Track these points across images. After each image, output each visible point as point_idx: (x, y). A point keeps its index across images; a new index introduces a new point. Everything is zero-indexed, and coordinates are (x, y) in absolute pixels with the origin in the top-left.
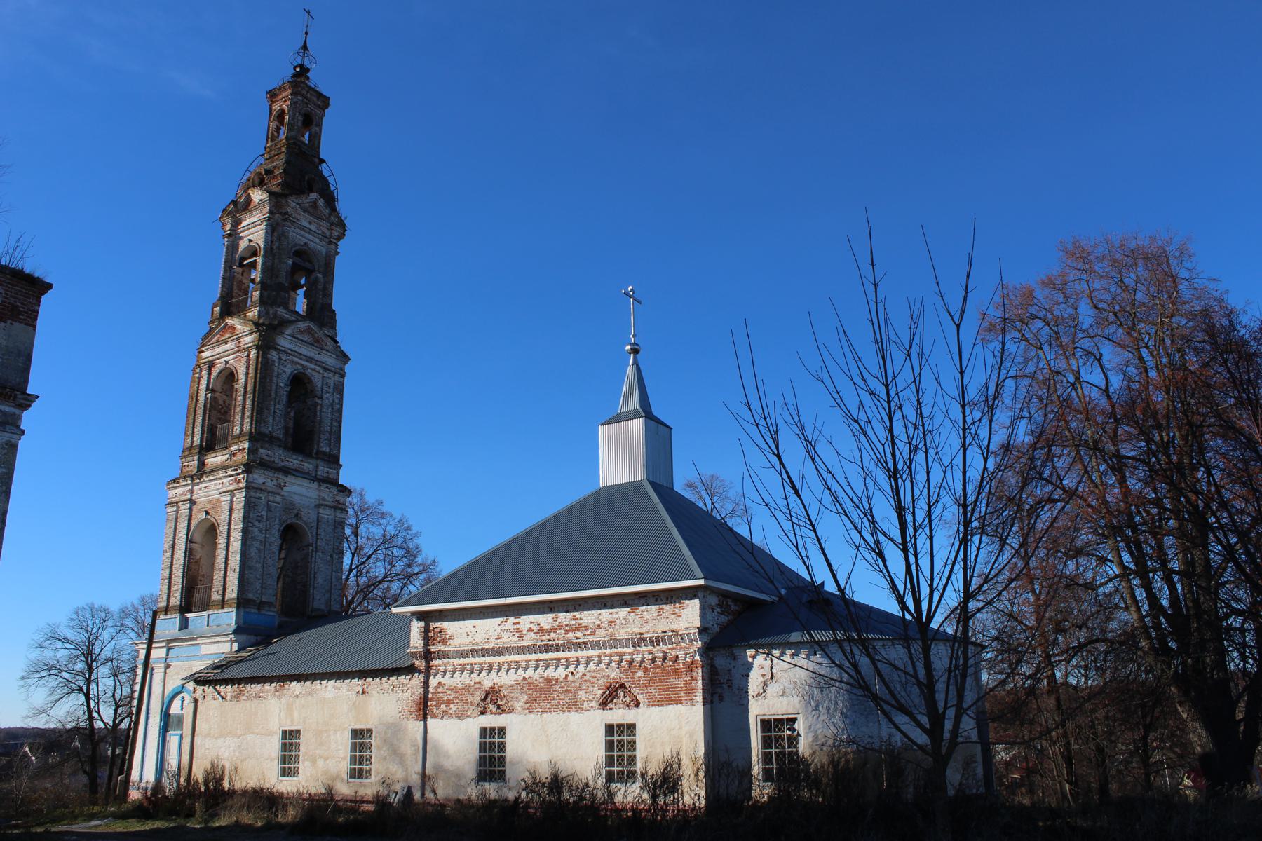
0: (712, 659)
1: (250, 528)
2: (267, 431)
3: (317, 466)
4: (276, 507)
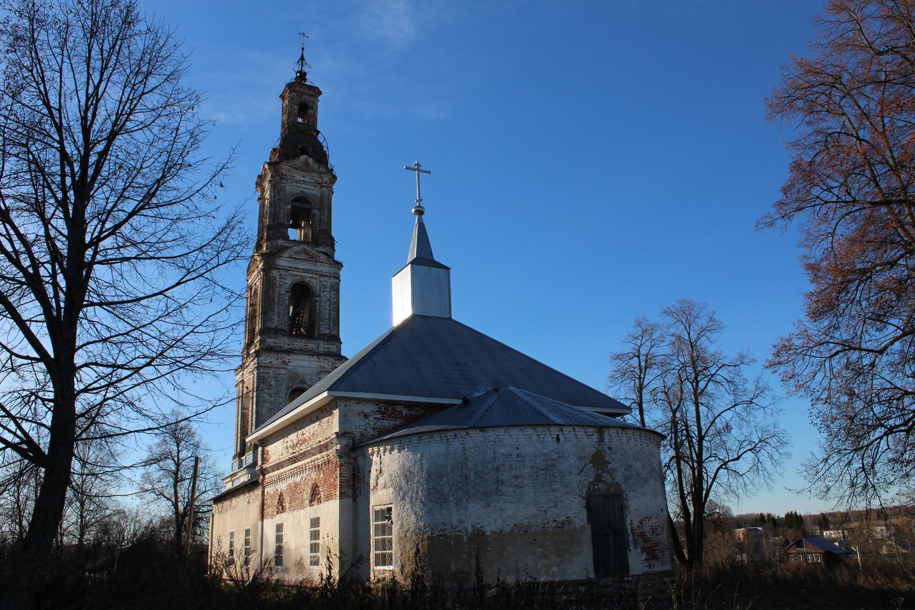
0: (355, 459)
1: (262, 395)
2: (273, 326)
3: (319, 344)
4: (282, 378)
